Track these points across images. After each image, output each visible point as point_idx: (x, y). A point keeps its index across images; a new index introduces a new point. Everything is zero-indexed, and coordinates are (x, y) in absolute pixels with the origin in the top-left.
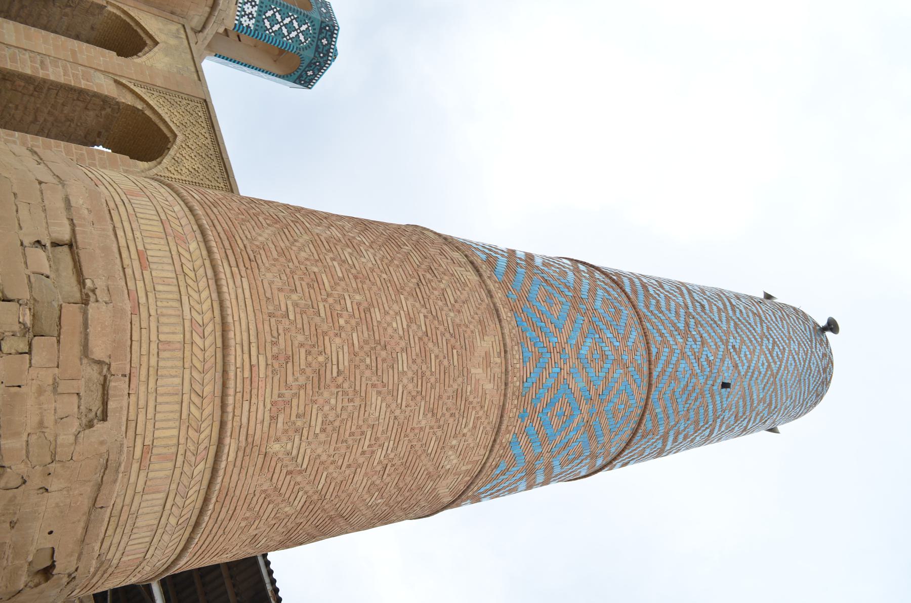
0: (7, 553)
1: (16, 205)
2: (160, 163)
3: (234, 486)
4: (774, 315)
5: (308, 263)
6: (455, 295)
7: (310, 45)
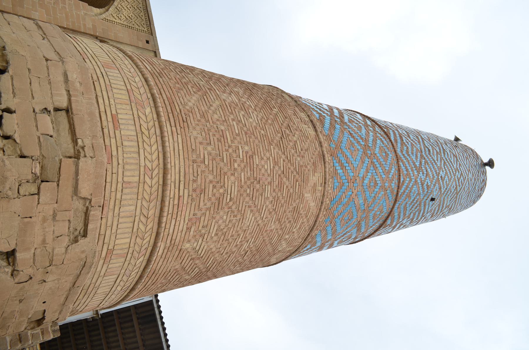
0: (15, 315)
1: (30, 78)
2: (107, 10)
3: (159, 268)
4: (463, 156)
5: (218, 123)
6: (301, 146)
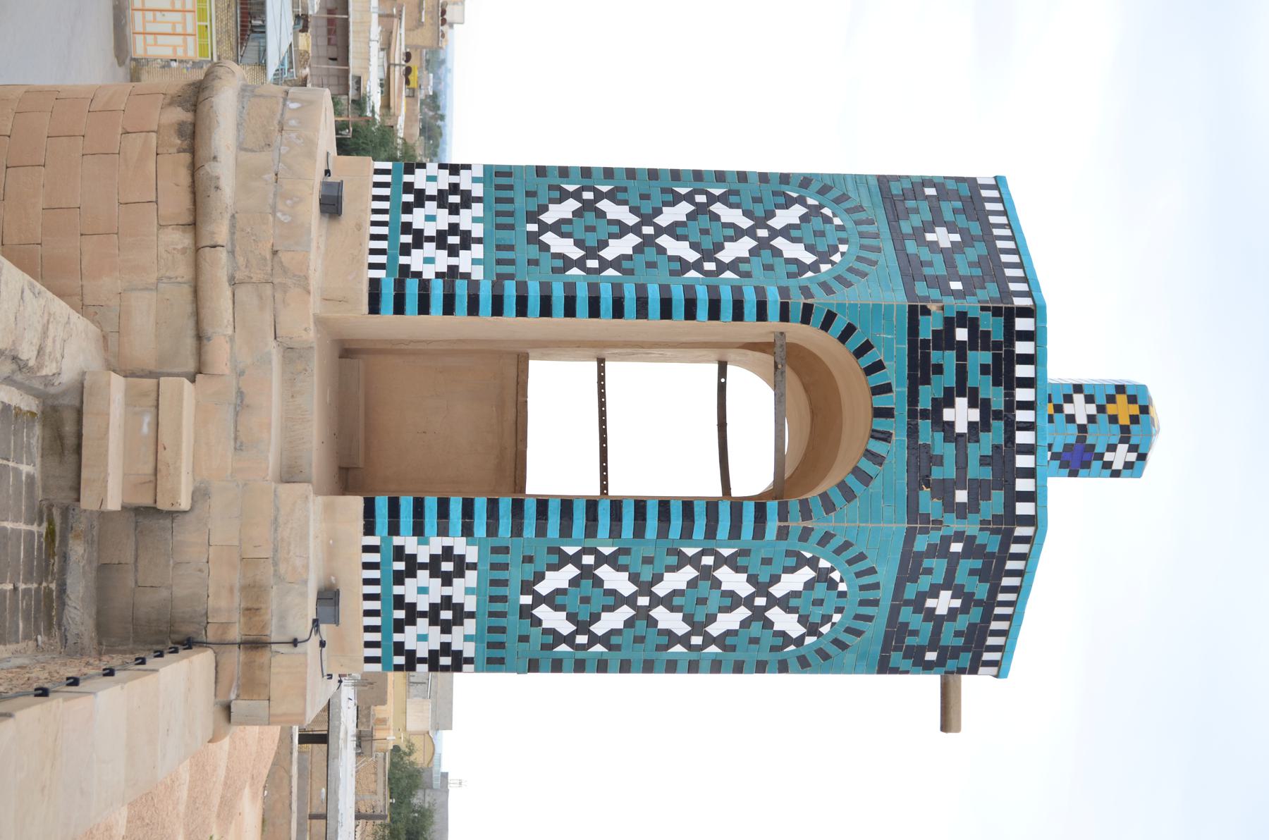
5: (175, 252)
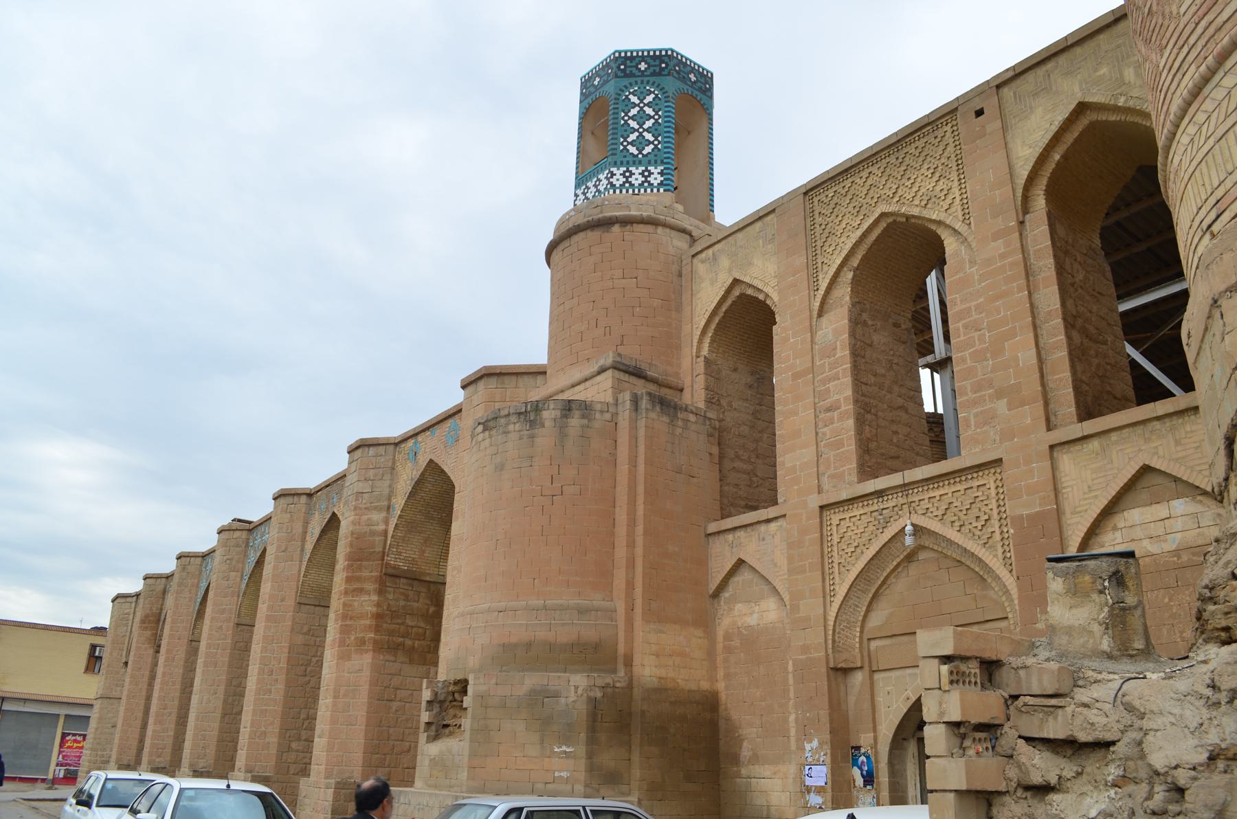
7: (656, 85)
